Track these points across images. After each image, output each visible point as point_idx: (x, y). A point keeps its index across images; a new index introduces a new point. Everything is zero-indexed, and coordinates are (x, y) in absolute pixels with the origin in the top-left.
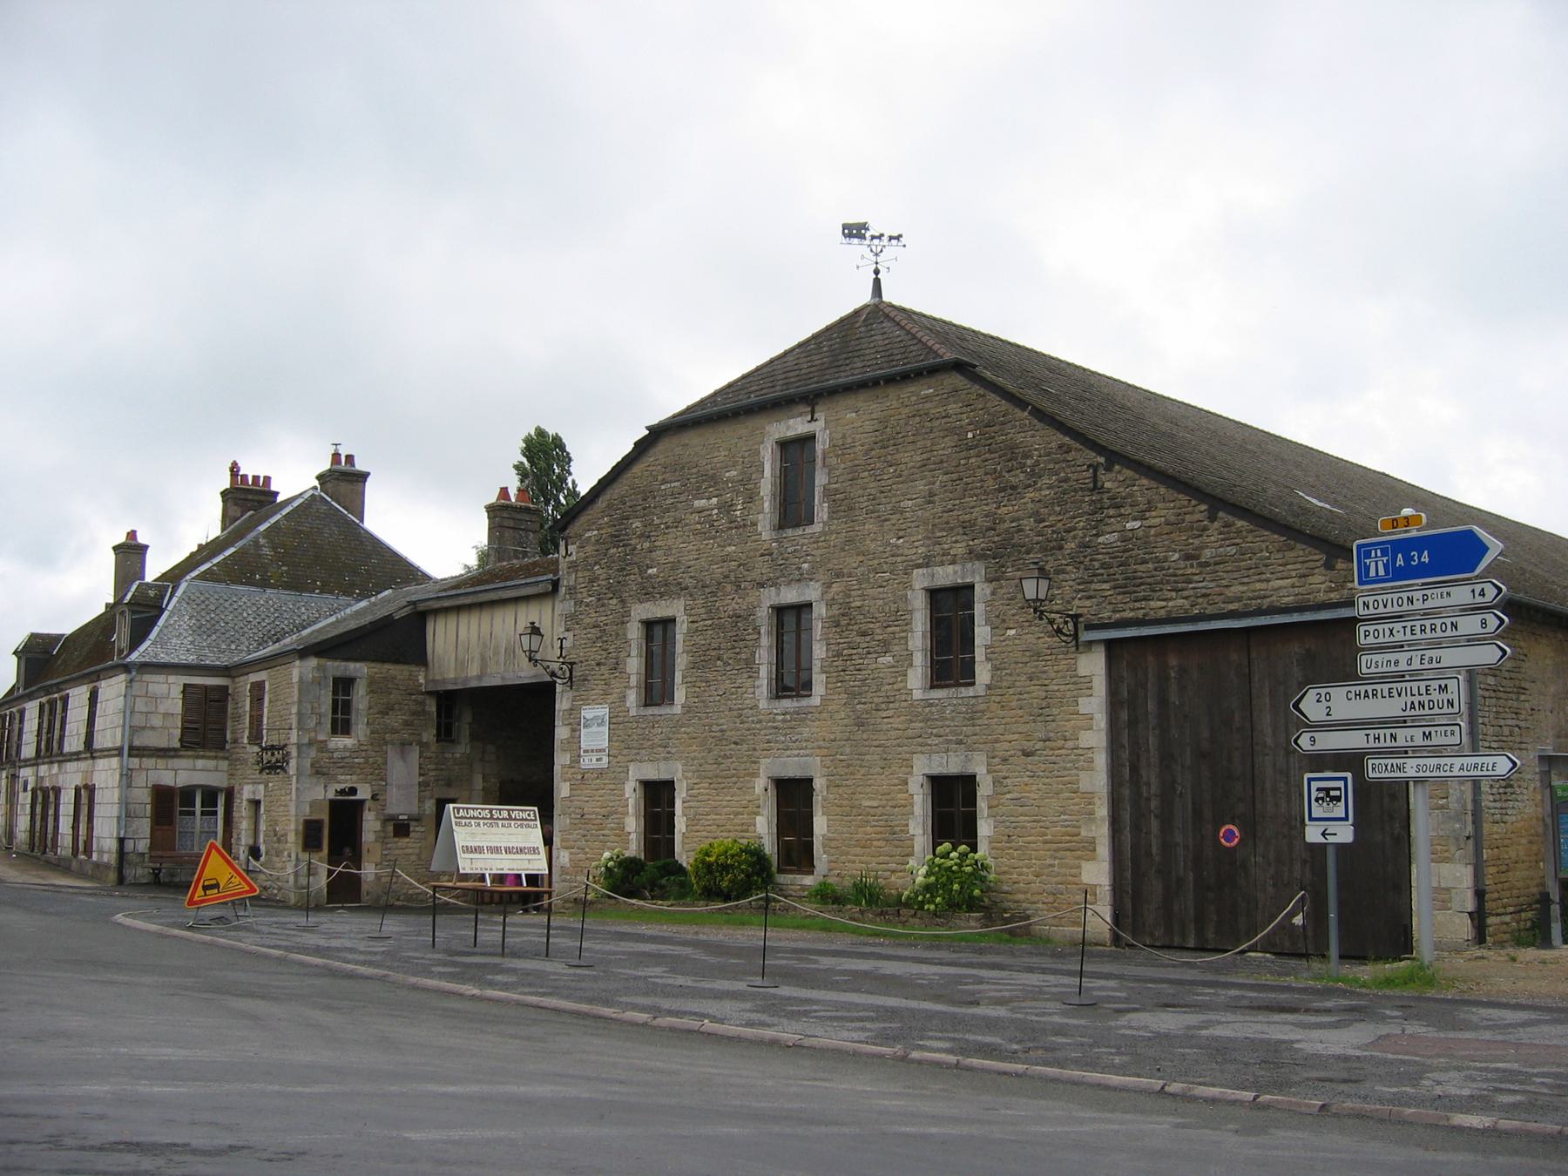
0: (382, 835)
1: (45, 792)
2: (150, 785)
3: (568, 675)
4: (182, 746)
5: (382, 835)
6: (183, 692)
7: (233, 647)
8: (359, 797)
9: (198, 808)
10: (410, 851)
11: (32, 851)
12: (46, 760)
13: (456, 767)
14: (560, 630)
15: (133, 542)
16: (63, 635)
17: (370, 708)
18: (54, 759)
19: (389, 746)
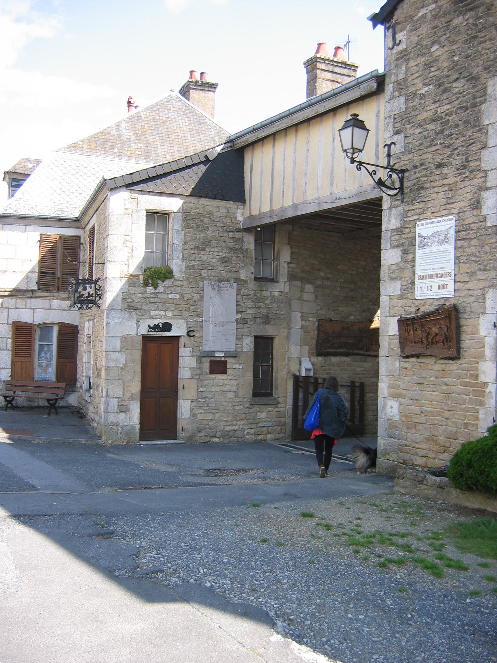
0: (198, 372)
2: (11, 322)
3: (397, 185)
5: (198, 372)
8: (173, 333)
10: (226, 388)
13: (275, 306)
14: (387, 136)
17: (186, 243)
19: (206, 283)
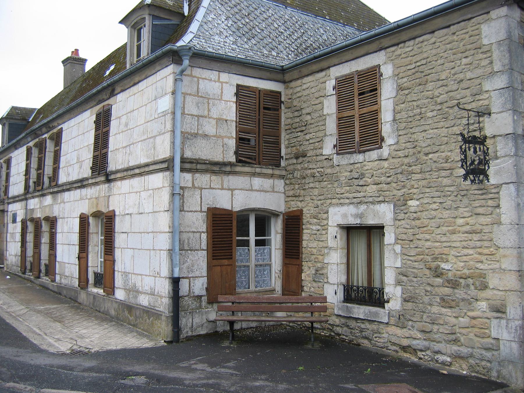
1: (37, 223)
2: (205, 209)
4: (239, 161)
6: (237, 94)
7: (274, 53)
9: (252, 237)
11: (24, 273)
12: (37, 194)
15: (77, 57)
16: (35, 109)
18: (45, 192)
